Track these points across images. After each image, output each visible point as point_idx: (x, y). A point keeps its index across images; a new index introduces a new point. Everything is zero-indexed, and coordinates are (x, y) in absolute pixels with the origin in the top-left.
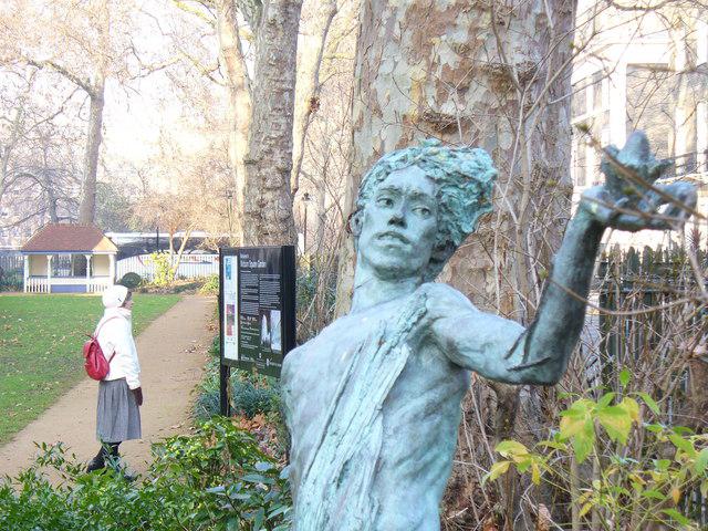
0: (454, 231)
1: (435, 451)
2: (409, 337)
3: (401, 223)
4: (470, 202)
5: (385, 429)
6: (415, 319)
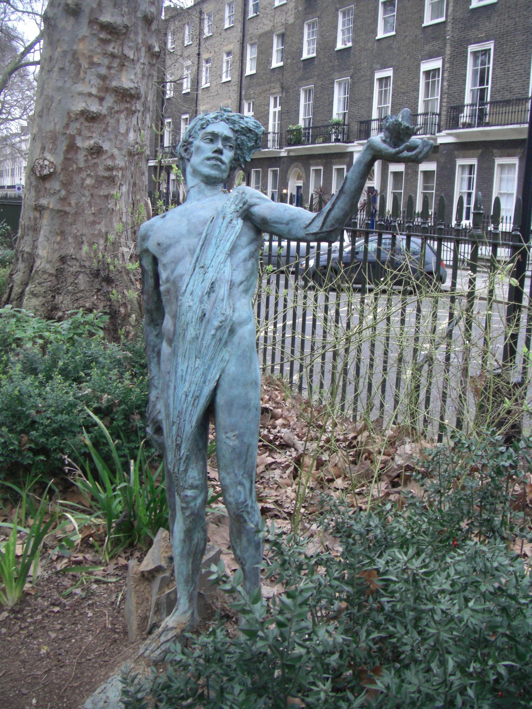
0: (242, 160)
3: (219, 152)
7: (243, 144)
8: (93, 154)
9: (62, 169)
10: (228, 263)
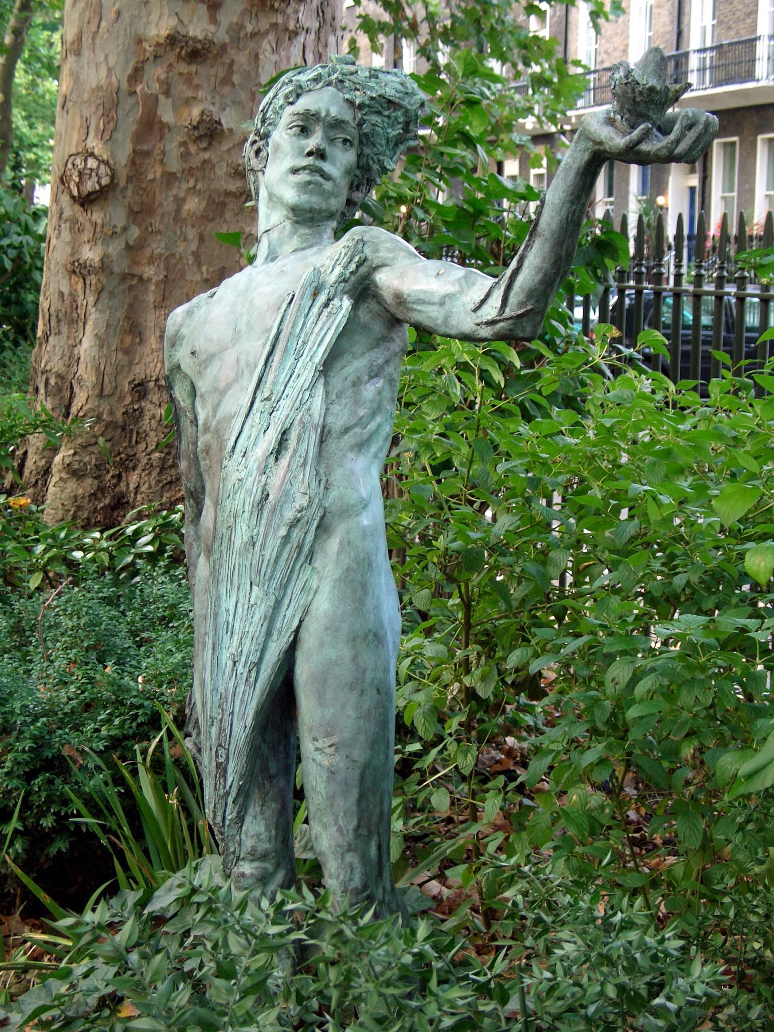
1: (378, 419)
2: (347, 289)
4: (395, 133)
5: (327, 394)
6: (353, 267)
7: (374, 133)
8: (200, 138)
9: (129, 179)
10: (320, 390)
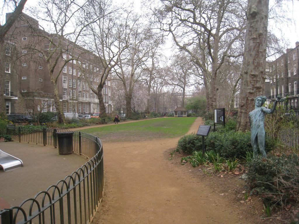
3: (259, 102)
